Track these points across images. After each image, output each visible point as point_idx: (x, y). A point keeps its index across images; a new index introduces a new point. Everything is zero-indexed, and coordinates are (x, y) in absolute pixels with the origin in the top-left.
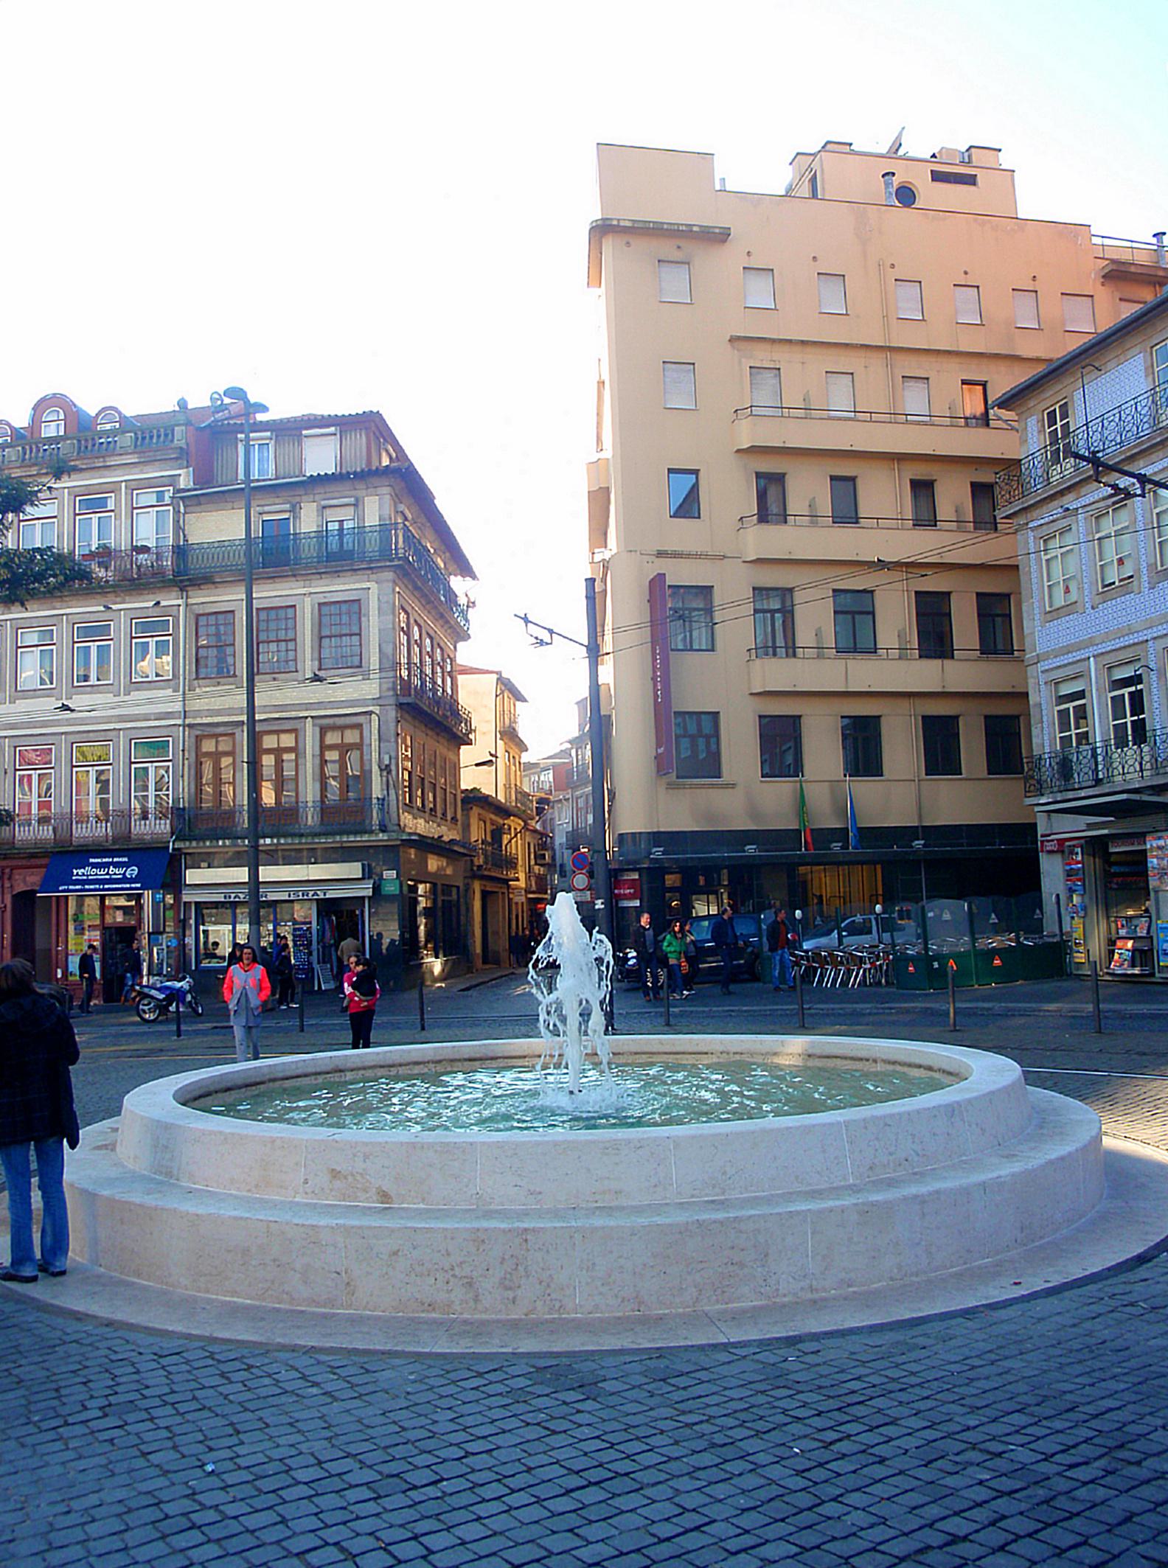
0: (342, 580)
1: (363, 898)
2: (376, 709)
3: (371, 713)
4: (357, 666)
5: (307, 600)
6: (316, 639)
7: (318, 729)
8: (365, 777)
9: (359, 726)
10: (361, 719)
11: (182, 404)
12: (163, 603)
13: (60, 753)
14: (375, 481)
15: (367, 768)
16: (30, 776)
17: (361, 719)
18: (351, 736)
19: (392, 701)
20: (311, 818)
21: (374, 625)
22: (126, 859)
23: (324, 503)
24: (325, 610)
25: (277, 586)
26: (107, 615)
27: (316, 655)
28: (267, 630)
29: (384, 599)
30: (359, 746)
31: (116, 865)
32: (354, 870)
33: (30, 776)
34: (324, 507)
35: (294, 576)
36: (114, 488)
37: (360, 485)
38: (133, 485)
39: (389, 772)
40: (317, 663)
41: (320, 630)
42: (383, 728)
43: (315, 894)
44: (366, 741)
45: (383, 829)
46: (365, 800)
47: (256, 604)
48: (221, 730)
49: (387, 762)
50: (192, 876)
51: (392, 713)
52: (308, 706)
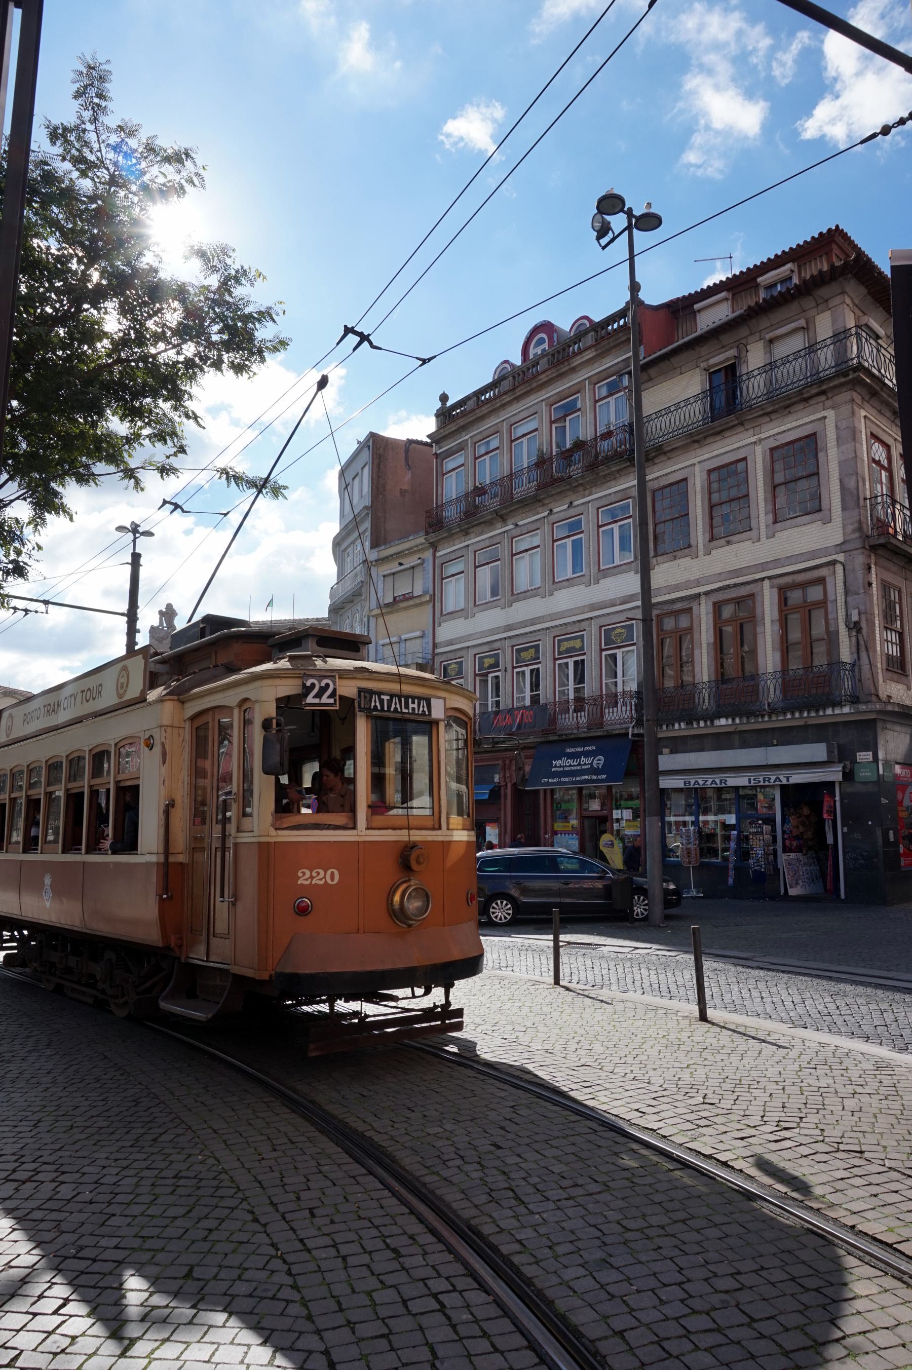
0: (794, 416)
1: (832, 784)
2: (840, 557)
3: (833, 563)
4: (814, 508)
5: (759, 449)
6: (770, 489)
7: (775, 591)
8: (832, 639)
9: (822, 581)
10: (823, 572)
11: (359, 442)
12: (555, 510)
13: (546, 648)
14: (824, 292)
15: (832, 628)
16: (523, 672)
17: (823, 572)
18: (815, 593)
19: (858, 544)
20: (772, 692)
21: (832, 459)
22: (593, 748)
23: (768, 336)
24: (776, 454)
25: (728, 441)
26: (573, 511)
27: (770, 507)
28: (719, 491)
29: (844, 424)
30: (823, 604)
31: (587, 754)
32: (817, 751)
33: (523, 672)
34: (771, 341)
35: (742, 424)
36: (578, 389)
37: (808, 303)
38: (594, 379)
39: (859, 631)
40: (771, 516)
41: (710, 499)
42: (849, 578)
43: (778, 779)
44: (831, 597)
45: (854, 700)
46: (835, 664)
47: (651, 486)
48: (678, 606)
49: (855, 618)
50: (666, 761)
51: (860, 559)
52: (763, 566)
